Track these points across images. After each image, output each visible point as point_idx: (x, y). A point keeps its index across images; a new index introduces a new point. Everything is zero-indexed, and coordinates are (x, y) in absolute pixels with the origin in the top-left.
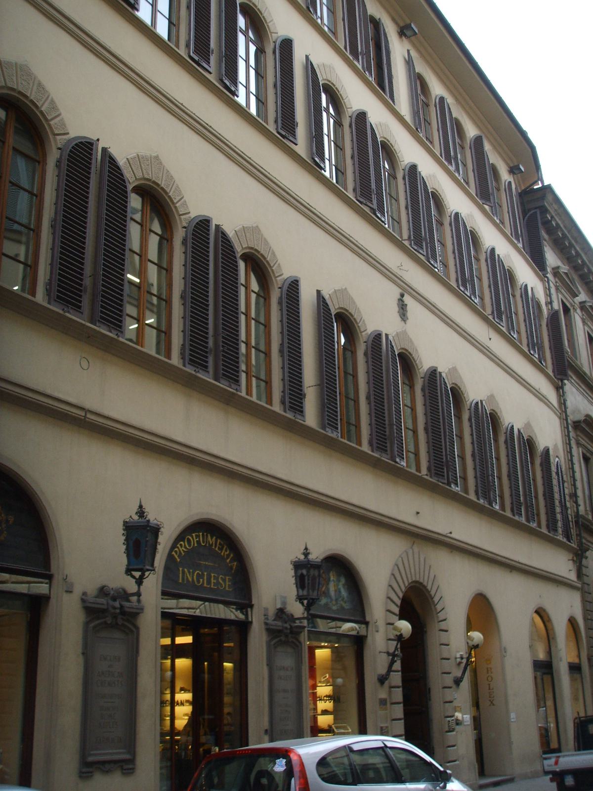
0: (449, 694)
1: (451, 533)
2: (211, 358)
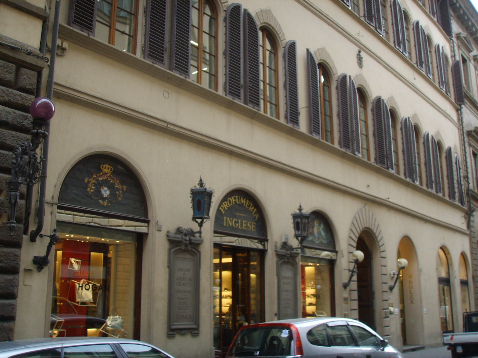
0: (386, 296)
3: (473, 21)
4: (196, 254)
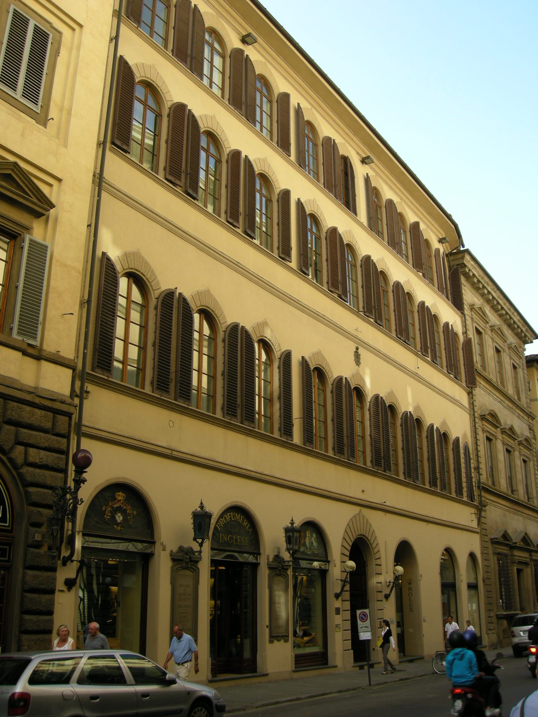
0: (378, 605)
1: (385, 502)
2: (237, 408)
3: (489, 289)
4: (195, 571)
